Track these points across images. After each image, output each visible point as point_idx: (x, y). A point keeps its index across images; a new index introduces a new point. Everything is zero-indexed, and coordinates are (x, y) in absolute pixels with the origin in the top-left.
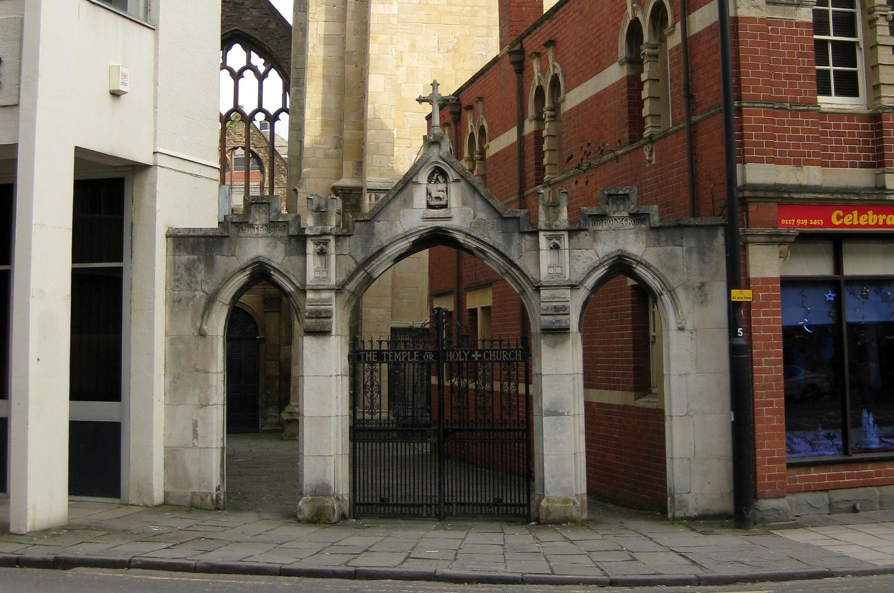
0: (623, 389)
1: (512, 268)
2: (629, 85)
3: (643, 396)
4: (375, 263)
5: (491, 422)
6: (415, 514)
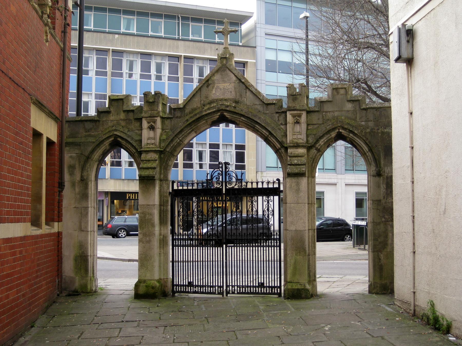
0: (25, 222)
5: (236, 234)
6: (211, 293)
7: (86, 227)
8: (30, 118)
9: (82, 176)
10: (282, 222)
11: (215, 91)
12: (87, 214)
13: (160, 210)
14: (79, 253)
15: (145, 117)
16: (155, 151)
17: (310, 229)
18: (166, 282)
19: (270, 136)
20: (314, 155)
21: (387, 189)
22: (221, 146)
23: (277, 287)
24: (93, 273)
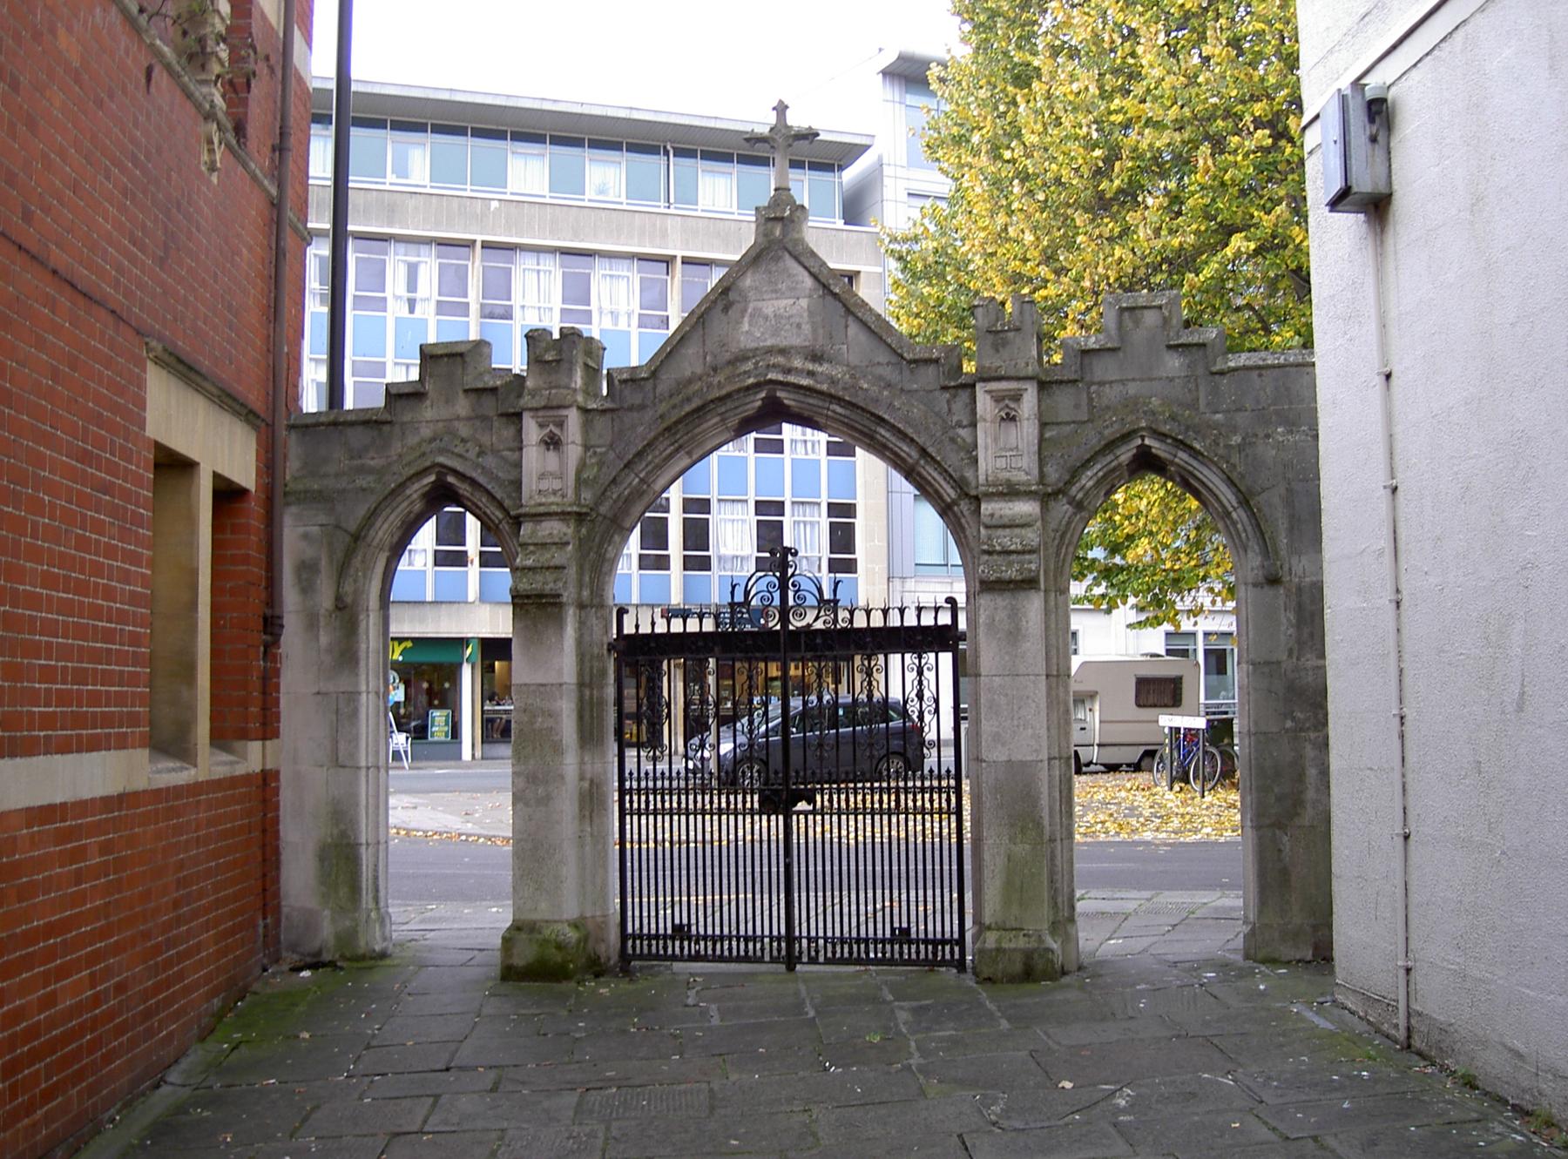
0: (122, 743)
7: (353, 755)
8: (144, 409)
9: (338, 598)
10: (965, 718)
11: (750, 325)
12: (355, 714)
13: (581, 700)
14: (332, 835)
15: (531, 409)
16: (563, 516)
17: (1055, 758)
18: (602, 926)
19: (922, 462)
20: (1064, 523)
21: (1299, 625)
22: (788, 508)
23: (950, 941)
24: (376, 899)
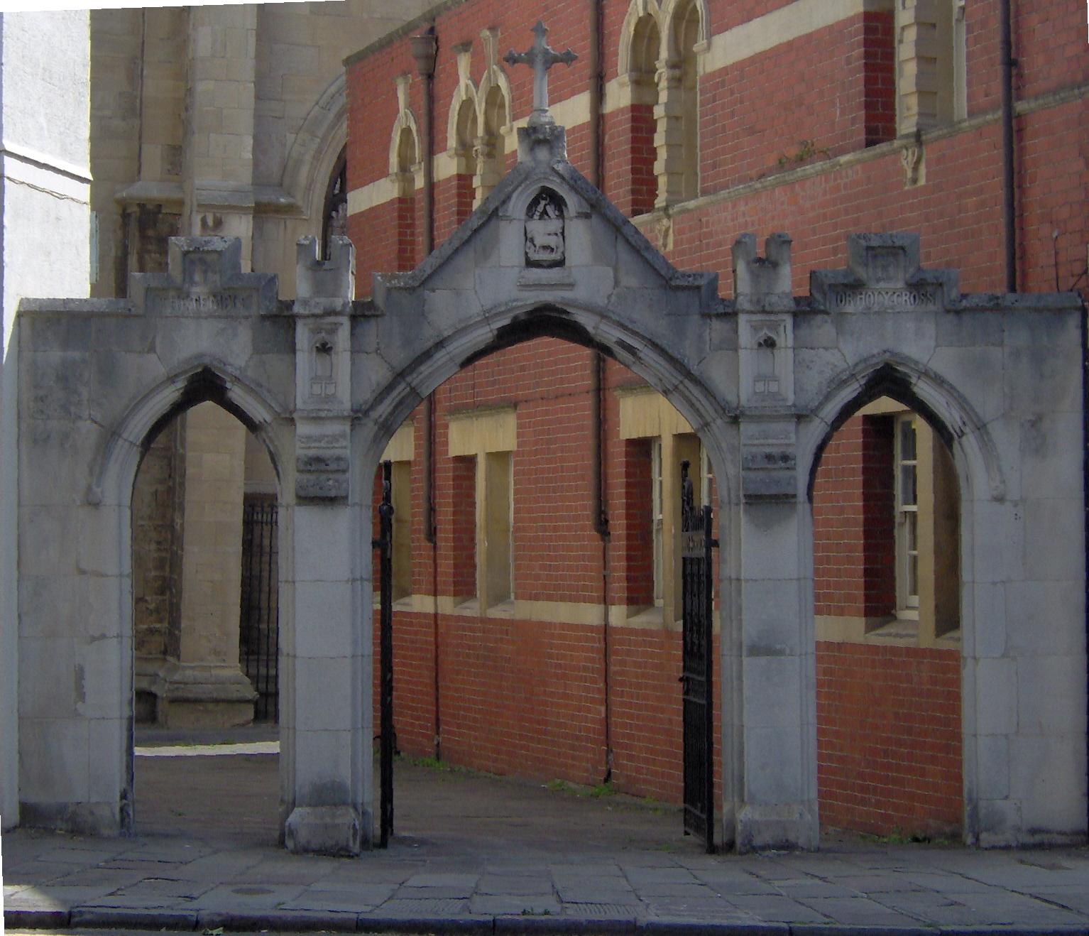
0: (841, 612)
1: (686, 381)
2: (868, 30)
3: (881, 625)
4: (425, 369)
